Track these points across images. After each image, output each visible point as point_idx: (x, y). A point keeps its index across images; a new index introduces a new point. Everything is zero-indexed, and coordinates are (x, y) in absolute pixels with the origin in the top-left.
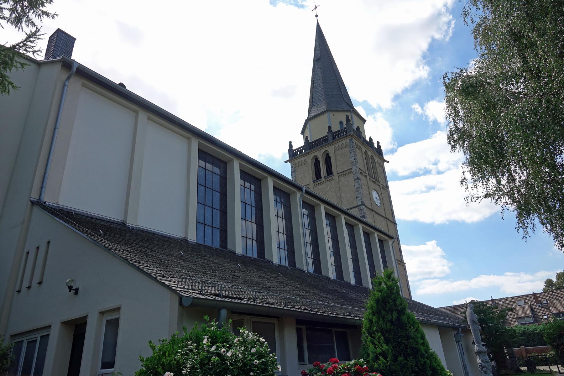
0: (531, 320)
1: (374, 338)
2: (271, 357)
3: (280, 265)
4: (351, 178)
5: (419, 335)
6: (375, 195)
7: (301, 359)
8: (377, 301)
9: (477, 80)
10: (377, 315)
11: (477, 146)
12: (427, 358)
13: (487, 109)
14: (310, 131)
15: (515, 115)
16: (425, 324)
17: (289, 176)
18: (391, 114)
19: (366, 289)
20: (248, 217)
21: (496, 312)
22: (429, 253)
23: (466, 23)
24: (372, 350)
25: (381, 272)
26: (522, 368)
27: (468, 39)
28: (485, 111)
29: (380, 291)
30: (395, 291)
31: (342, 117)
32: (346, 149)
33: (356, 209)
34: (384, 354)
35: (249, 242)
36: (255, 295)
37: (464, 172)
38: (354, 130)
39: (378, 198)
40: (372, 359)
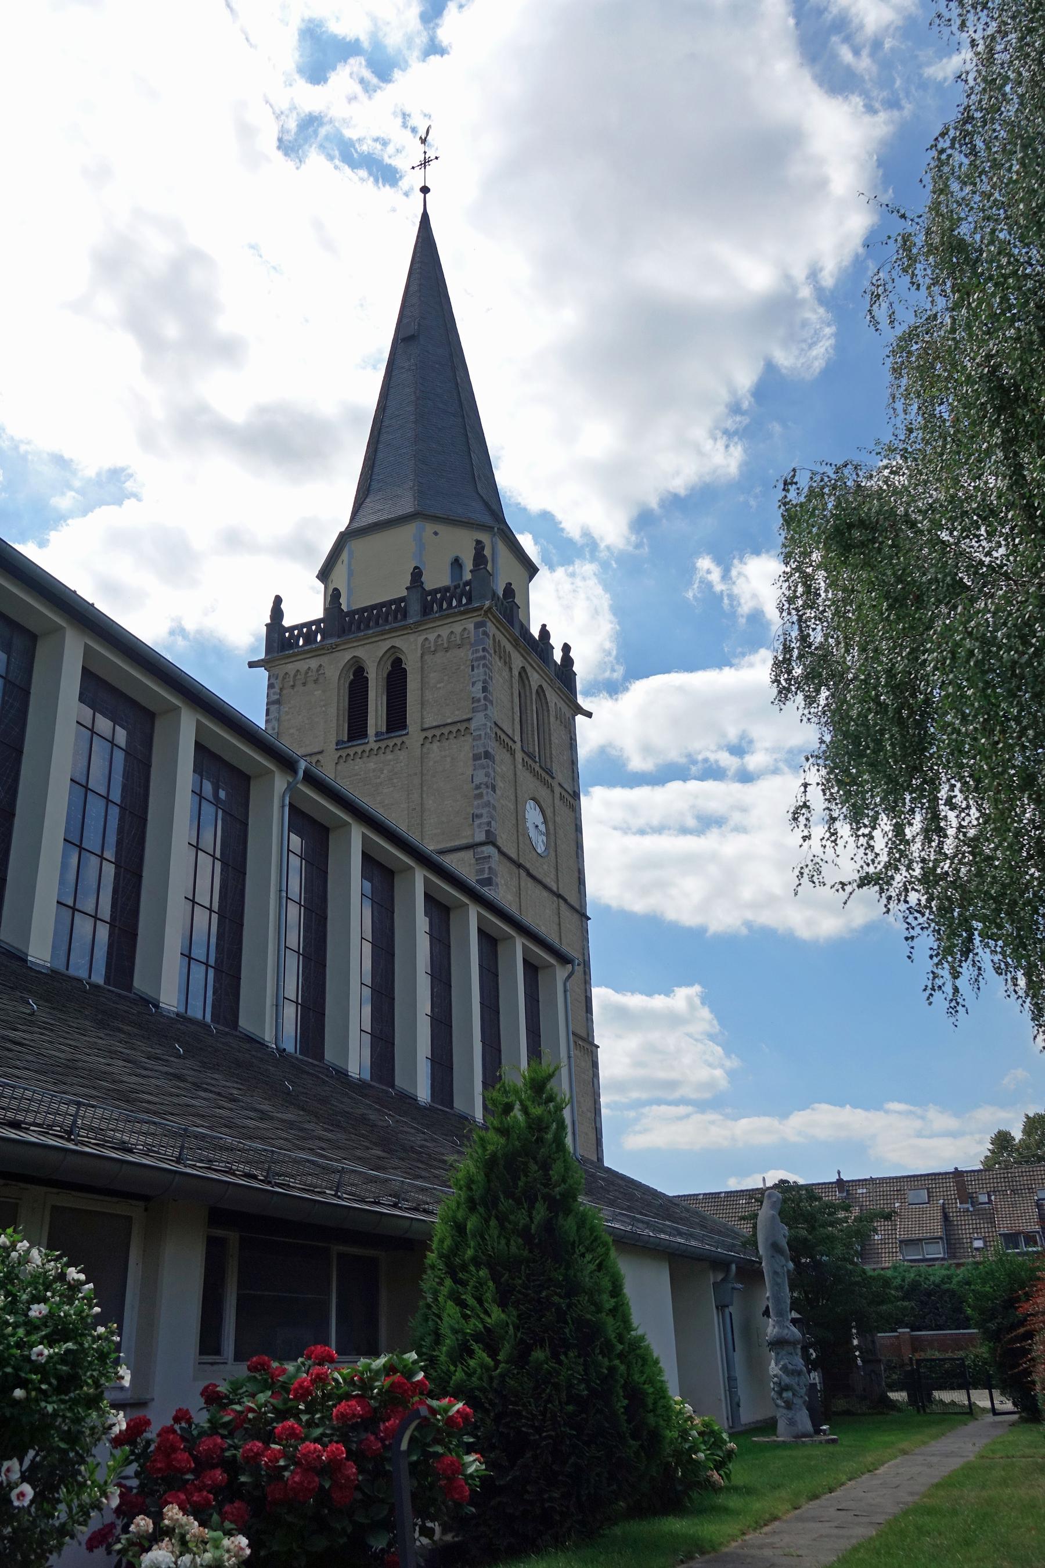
0: (937, 1251)
1: (463, 1283)
2: (99, 1337)
3: (182, 1018)
4: (462, 749)
5: (606, 1283)
6: (533, 816)
7: (209, 1343)
8: (490, 1165)
9: (881, 506)
10: (481, 1210)
11: (854, 713)
12: (621, 1356)
13: (897, 602)
14: (351, 574)
15: (970, 634)
16: (633, 1245)
17: (257, 717)
18: (622, 572)
19: (465, 1119)
20: (92, 841)
21: (845, 1220)
22: (673, 1020)
23: (874, 322)
24: (452, 1322)
25: (518, 1065)
26: (893, 1396)
27: (879, 377)
28: (890, 607)
29: (504, 1131)
30: (549, 1136)
31: (461, 543)
32: (461, 653)
33: (467, 855)
34: (489, 1340)
35: (84, 926)
36: (76, 1116)
37: (806, 785)
38: (494, 594)
39: (542, 828)
40: (449, 1355)
